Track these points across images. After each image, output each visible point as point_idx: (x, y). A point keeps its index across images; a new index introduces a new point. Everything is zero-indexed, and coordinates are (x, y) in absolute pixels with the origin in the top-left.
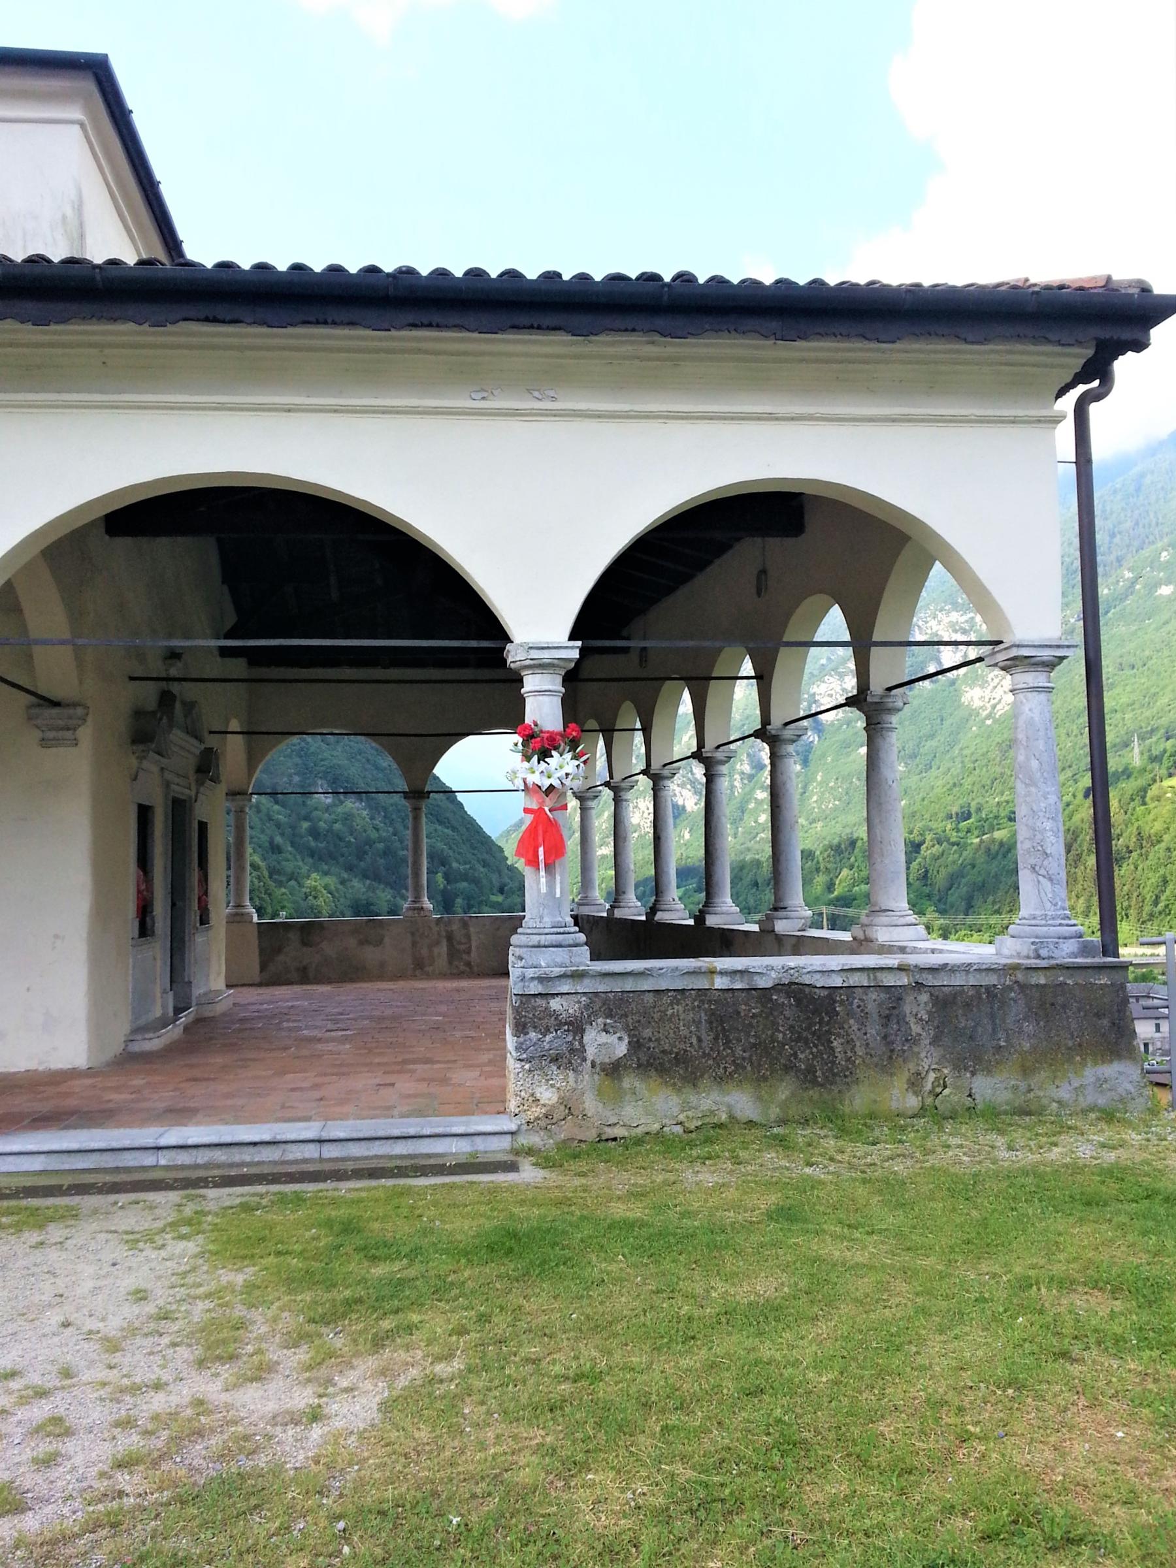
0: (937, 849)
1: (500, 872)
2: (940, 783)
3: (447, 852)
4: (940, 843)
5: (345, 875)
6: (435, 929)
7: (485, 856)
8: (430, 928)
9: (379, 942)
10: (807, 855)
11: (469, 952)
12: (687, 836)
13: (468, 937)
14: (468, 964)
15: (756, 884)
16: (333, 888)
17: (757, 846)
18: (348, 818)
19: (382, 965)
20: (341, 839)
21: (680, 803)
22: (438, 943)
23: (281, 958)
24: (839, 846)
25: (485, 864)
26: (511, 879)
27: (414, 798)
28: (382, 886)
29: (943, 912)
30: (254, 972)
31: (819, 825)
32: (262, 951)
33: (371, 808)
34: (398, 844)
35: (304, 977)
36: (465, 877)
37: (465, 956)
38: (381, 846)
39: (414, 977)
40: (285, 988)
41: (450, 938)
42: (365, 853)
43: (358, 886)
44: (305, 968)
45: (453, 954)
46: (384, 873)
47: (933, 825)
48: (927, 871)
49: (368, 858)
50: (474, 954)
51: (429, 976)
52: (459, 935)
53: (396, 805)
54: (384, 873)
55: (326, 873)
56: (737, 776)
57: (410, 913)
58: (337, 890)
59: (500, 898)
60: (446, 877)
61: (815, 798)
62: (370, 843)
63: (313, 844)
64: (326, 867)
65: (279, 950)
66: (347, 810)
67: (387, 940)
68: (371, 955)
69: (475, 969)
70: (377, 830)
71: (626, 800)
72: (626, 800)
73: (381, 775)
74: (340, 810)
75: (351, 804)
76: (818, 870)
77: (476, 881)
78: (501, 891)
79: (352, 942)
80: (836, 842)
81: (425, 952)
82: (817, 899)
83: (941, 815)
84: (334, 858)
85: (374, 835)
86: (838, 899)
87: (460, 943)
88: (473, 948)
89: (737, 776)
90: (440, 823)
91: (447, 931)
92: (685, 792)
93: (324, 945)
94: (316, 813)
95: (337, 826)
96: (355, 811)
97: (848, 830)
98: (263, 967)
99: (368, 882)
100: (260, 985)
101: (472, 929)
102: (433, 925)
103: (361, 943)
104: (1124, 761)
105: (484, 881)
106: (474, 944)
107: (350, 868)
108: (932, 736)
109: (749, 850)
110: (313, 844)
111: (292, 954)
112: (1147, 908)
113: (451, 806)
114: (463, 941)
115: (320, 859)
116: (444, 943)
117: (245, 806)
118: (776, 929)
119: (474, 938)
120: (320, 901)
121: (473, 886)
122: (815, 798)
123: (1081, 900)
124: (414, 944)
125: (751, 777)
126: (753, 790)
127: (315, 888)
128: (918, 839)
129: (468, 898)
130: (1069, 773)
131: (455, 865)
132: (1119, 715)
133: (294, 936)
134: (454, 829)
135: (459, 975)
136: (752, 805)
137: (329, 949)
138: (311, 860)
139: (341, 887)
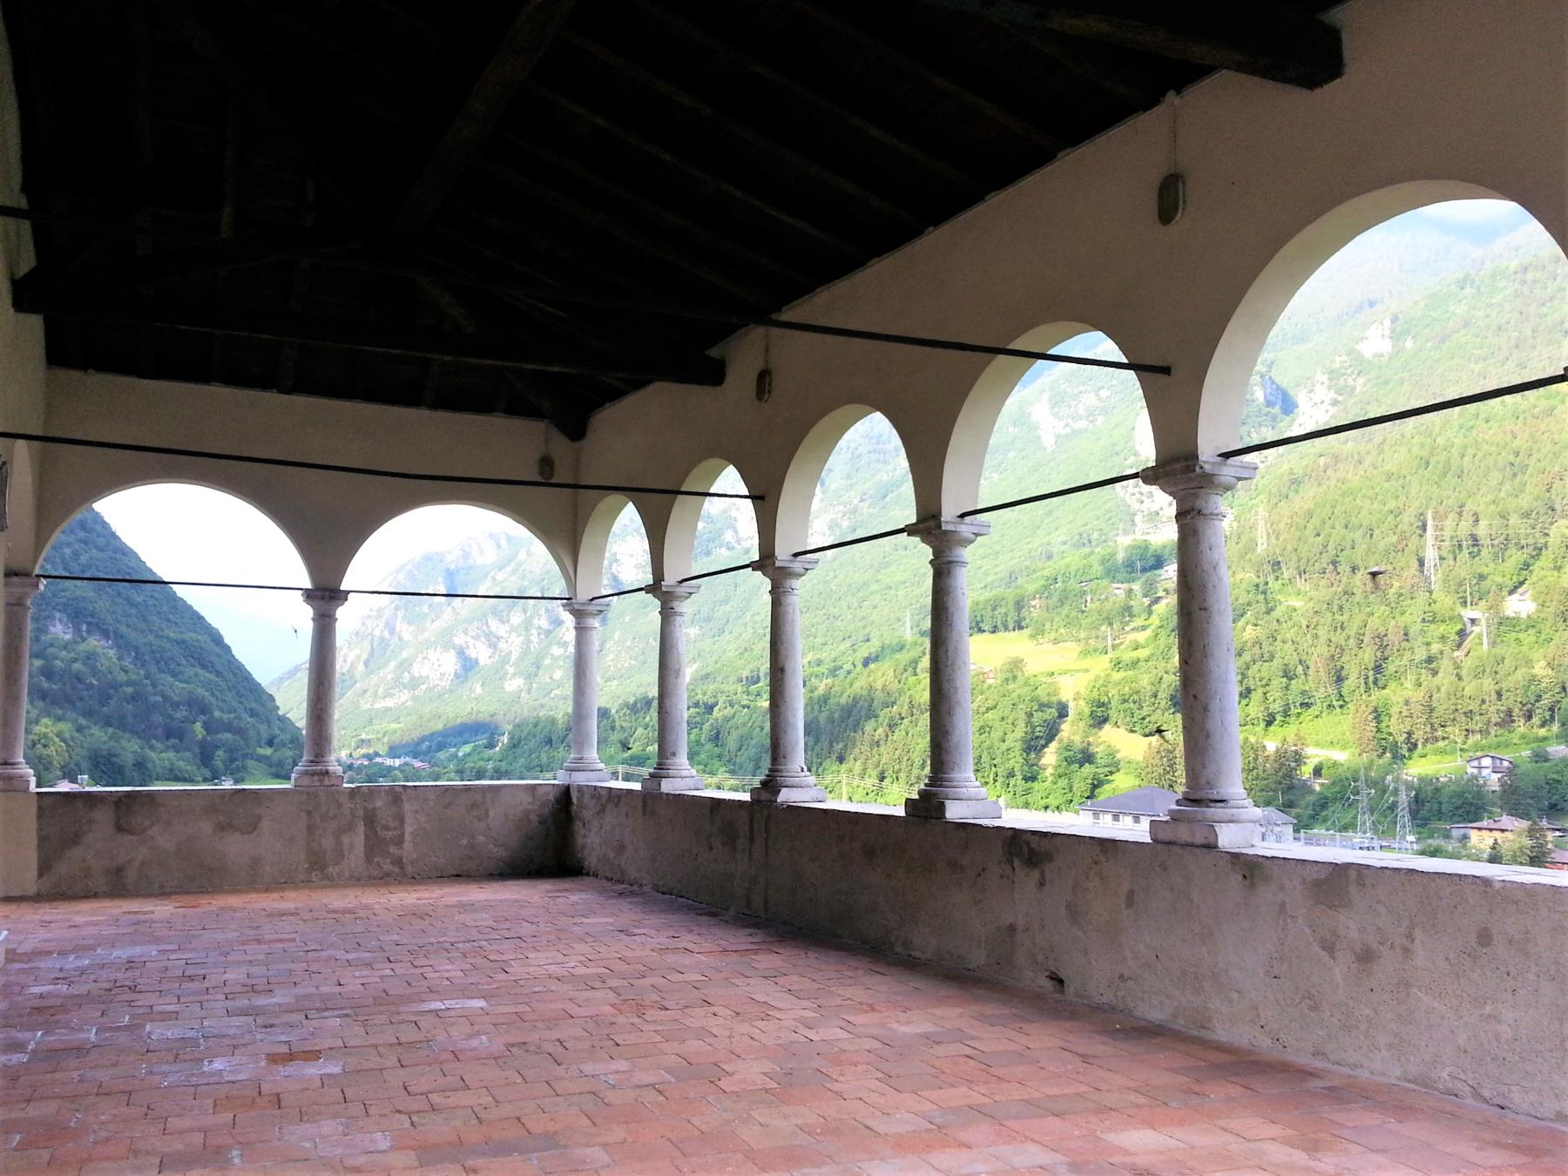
0: (729, 711)
1: (269, 722)
2: (732, 647)
3: (210, 699)
4: (732, 705)
5: (82, 721)
6: (347, 805)
7: (254, 705)
8: (340, 806)
9: (253, 826)
10: (604, 713)
11: (399, 841)
12: (479, 690)
13: (401, 819)
14: (398, 862)
15: (550, 742)
16: (67, 735)
17: (552, 703)
18: (90, 657)
19: (256, 862)
20: (80, 680)
21: (473, 656)
22: (350, 828)
23: (76, 853)
24: (635, 703)
25: (253, 713)
26: (282, 730)
27: (323, 598)
28: (127, 735)
29: (733, 772)
30: (29, 880)
31: (615, 683)
32: (42, 839)
33: (119, 647)
34: (150, 688)
35: (118, 885)
36: (229, 728)
37: (393, 849)
38: (130, 690)
39: (306, 884)
40: (85, 906)
41: (370, 820)
42: (109, 697)
43: (99, 735)
44: (119, 870)
45: (374, 844)
46: (130, 720)
47: (725, 687)
48: (718, 733)
49: (112, 703)
50: (407, 845)
51: (333, 882)
52: (385, 815)
53: (150, 644)
54: (130, 720)
55: (59, 719)
56: (534, 631)
57: (306, 781)
58: (73, 738)
59: (268, 751)
60: (206, 726)
61: (611, 656)
62: (116, 686)
63: (45, 685)
64: (60, 712)
65: (75, 839)
66: (89, 648)
67: (265, 825)
68: (236, 847)
69: (409, 869)
70: (126, 672)
71: (681, 614)
72: (681, 614)
73: (133, 611)
74: (82, 647)
75: (94, 643)
76: (613, 728)
77: (240, 732)
78: (270, 743)
79: (206, 827)
80: (632, 701)
81: (328, 843)
82: (612, 757)
83: (733, 678)
84: (72, 703)
85: (122, 677)
86: (632, 758)
87: (386, 828)
88: (408, 837)
89: (534, 631)
90: (204, 667)
91: (365, 809)
92: (478, 644)
93: (155, 831)
94: (52, 650)
95: (77, 666)
96: (99, 650)
97: (642, 690)
98: (44, 868)
99: (111, 730)
100: (37, 898)
101: (407, 806)
102: (344, 800)
103: (222, 828)
104: (897, 634)
105: (252, 733)
106: (408, 830)
107: (89, 714)
108: (726, 601)
109: (542, 706)
110: (45, 685)
111: (99, 844)
112: (915, 772)
113: (216, 649)
114: (392, 825)
115: (53, 702)
116: (361, 829)
117: (26, 595)
118: (1220, 844)
119: (409, 819)
120: (52, 750)
121: (237, 738)
122: (611, 656)
123: (858, 763)
124: (311, 829)
125: (548, 633)
126: (550, 645)
127: (45, 736)
128: (711, 701)
129: (231, 750)
130: (848, 643)
131: (217, 714)
132: (892, 592)
133: (103, 816)
134: (218, 674)
135: (383, 880)
136: (547, 661)
137: (163, 838)
138: (41, 704)
139: (76, 735)
